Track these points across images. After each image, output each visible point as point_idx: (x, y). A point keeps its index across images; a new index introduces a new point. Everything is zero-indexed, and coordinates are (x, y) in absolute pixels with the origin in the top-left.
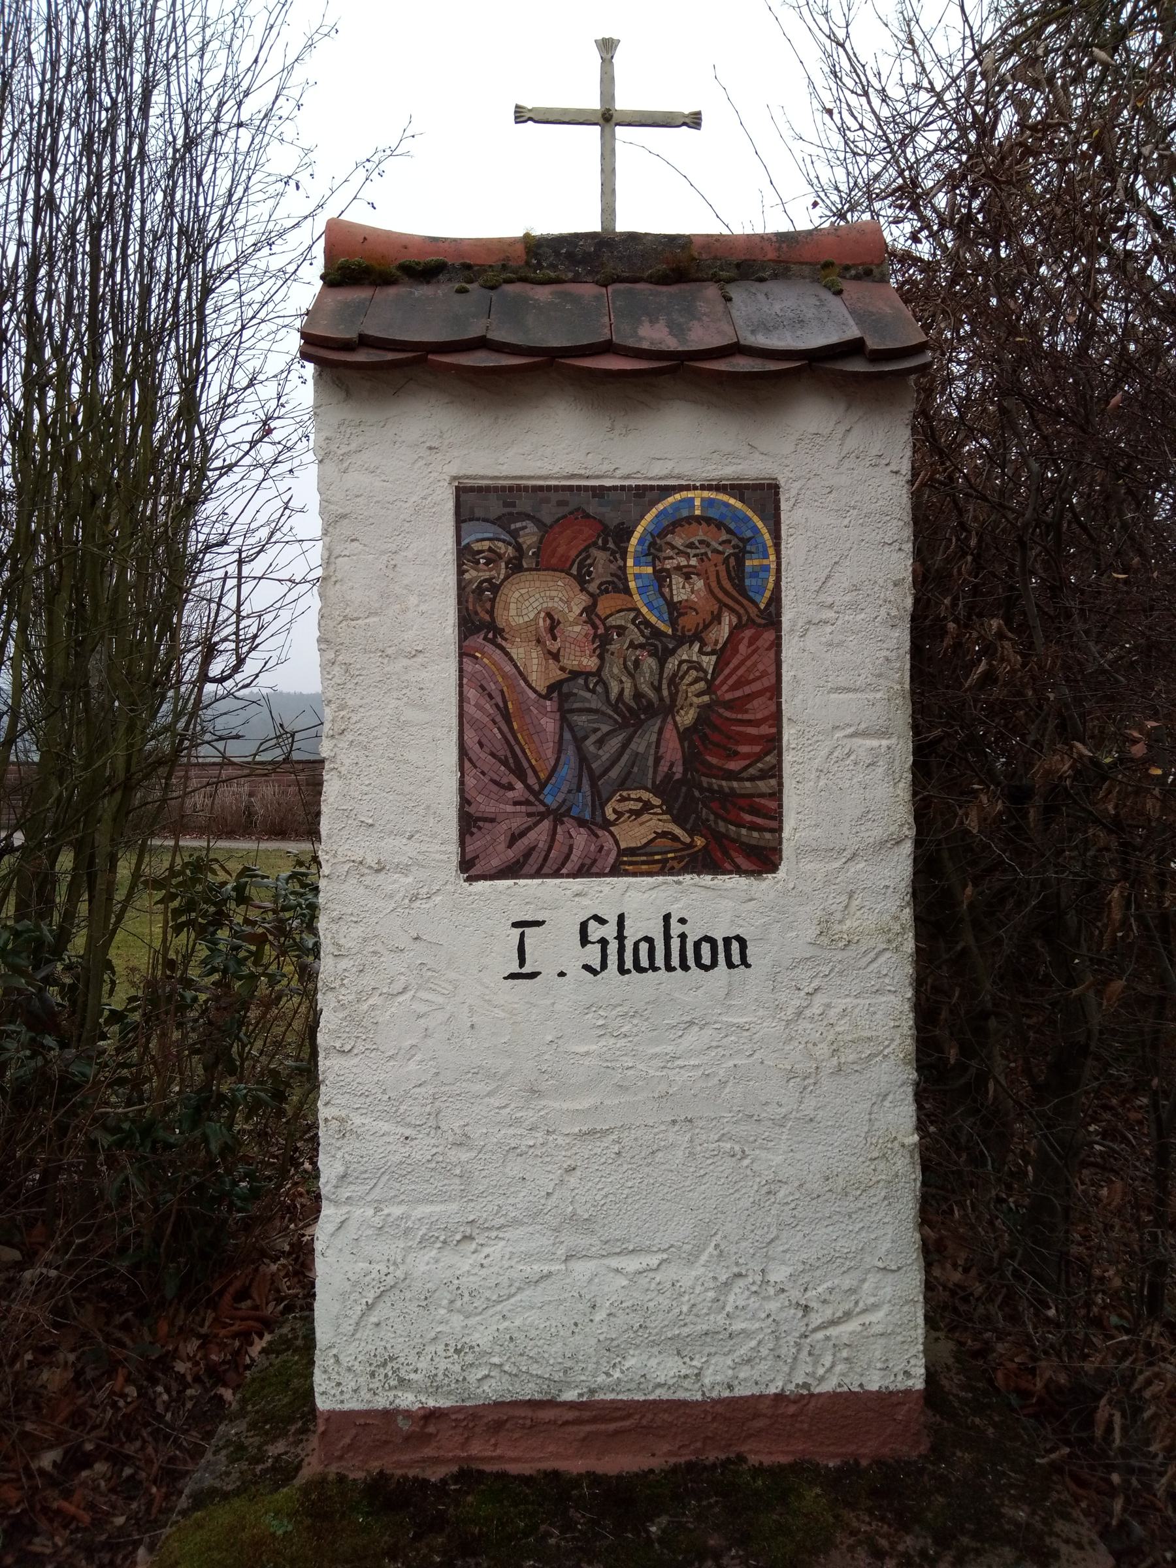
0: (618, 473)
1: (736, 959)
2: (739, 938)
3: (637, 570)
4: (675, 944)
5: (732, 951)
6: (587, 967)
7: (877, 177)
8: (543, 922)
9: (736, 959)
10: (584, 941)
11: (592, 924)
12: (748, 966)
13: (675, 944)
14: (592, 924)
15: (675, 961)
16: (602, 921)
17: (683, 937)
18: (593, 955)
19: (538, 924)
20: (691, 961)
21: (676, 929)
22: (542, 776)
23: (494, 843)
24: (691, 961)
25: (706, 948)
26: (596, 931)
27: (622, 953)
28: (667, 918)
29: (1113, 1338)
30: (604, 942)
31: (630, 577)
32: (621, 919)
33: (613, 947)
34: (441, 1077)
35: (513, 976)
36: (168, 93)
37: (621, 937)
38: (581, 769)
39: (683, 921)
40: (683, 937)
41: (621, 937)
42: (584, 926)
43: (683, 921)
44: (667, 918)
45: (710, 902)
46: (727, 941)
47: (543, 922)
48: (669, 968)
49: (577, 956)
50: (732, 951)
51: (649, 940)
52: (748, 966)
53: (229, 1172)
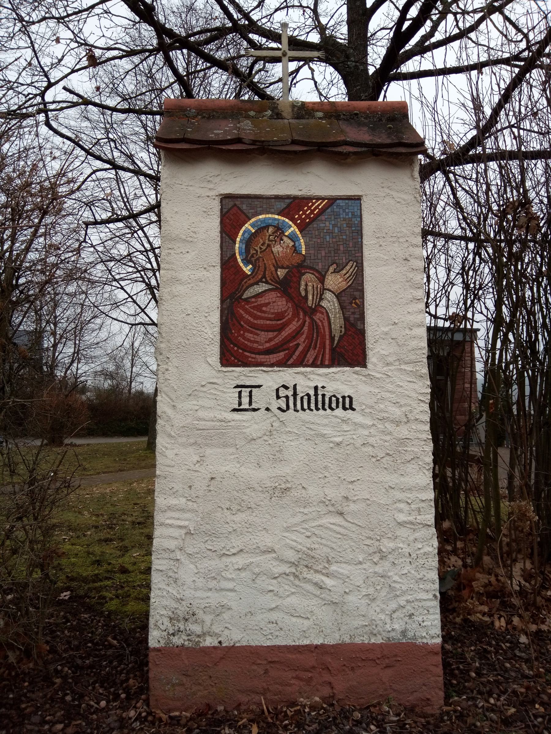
0: (236, 374)
1: (347, 406)
2: (349, 397)
3: (292, 229)
4: (320, 398)
5: (347, 403)
6: (279, 409)
8: (261, 386)
9: (347, 406)
10: (278, 397)
12: (354, 410)
13: (320, 398)
15: (320, 406)
16: (286, 388)
17: (324, 395)
18: (282, 403)
19: (259, 386)
21: (320, 393)
22: (312, 8)
25: (334, 405)
27: (293, 400)
28: (316, 388)
30: (287, 397)
31: (293, 225)
32: (295, 386)
35: (235, 410)
37: (295, 395)
40: (324, 395)
41: (295, 395)
42: (277, 390)
43: (323, 387)
44: (316, 388)
45: (337, 380)
47: (261, 386)
48: (317, 409)
49: (275, 404)
50: (347, 403)
51: (308, 395)
52: (354, 410)
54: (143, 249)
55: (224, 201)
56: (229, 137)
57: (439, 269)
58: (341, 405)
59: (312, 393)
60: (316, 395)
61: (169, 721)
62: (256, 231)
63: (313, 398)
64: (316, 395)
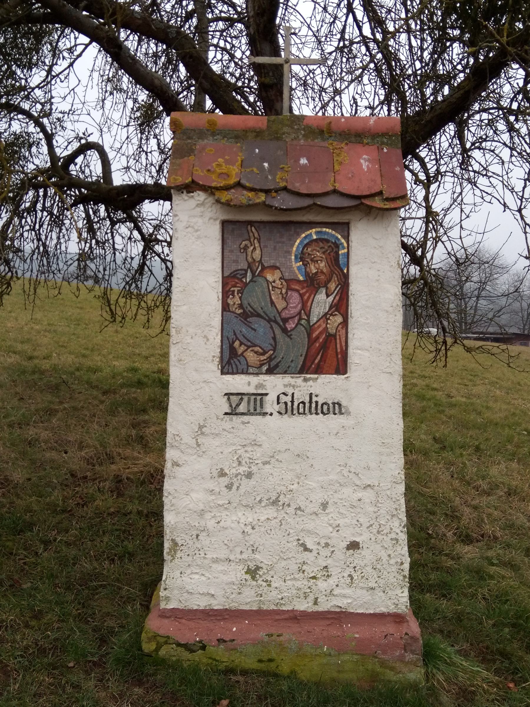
2: (338, 403)
4: (314, 405)
5: (336, 408)
7: (523, 317)
10: (278, 403)
11: (282, 396)
13: (314, 405)
14: (282, 396)
20: (319, 411)
21: (314, 399)
23: (231, 361)
24: (319, 411)
25: (325, 407)
26: (283, 398)
27: (290, 408)
28: (311, 395)
29: (238, 294)
30: (286, 403)
32: (293, 394)
33: (289, 404)
34: (221, 524)
36: (334, 298)
37: (292, 402)
38: (255, 311)
39: (317, 396)
40: (317, 402)
41: (292, 402)
42: (278, 397)
43: (317, 396)
44: (311, 395)
45: (325, 386)
46: (334, 404)
50: (336, 408)
53: (11, 186)
54: (272, 323)
55: (225, 225)
56: (201, 183)
57: (443, 138)
58: (331, 412)
59: (307, 400)
60: (310, 402)
61: (117, 282)
62: (316, 239)
63: (307, 405)
64: (310, 402)
